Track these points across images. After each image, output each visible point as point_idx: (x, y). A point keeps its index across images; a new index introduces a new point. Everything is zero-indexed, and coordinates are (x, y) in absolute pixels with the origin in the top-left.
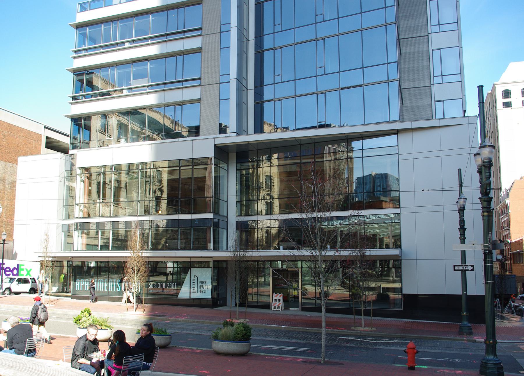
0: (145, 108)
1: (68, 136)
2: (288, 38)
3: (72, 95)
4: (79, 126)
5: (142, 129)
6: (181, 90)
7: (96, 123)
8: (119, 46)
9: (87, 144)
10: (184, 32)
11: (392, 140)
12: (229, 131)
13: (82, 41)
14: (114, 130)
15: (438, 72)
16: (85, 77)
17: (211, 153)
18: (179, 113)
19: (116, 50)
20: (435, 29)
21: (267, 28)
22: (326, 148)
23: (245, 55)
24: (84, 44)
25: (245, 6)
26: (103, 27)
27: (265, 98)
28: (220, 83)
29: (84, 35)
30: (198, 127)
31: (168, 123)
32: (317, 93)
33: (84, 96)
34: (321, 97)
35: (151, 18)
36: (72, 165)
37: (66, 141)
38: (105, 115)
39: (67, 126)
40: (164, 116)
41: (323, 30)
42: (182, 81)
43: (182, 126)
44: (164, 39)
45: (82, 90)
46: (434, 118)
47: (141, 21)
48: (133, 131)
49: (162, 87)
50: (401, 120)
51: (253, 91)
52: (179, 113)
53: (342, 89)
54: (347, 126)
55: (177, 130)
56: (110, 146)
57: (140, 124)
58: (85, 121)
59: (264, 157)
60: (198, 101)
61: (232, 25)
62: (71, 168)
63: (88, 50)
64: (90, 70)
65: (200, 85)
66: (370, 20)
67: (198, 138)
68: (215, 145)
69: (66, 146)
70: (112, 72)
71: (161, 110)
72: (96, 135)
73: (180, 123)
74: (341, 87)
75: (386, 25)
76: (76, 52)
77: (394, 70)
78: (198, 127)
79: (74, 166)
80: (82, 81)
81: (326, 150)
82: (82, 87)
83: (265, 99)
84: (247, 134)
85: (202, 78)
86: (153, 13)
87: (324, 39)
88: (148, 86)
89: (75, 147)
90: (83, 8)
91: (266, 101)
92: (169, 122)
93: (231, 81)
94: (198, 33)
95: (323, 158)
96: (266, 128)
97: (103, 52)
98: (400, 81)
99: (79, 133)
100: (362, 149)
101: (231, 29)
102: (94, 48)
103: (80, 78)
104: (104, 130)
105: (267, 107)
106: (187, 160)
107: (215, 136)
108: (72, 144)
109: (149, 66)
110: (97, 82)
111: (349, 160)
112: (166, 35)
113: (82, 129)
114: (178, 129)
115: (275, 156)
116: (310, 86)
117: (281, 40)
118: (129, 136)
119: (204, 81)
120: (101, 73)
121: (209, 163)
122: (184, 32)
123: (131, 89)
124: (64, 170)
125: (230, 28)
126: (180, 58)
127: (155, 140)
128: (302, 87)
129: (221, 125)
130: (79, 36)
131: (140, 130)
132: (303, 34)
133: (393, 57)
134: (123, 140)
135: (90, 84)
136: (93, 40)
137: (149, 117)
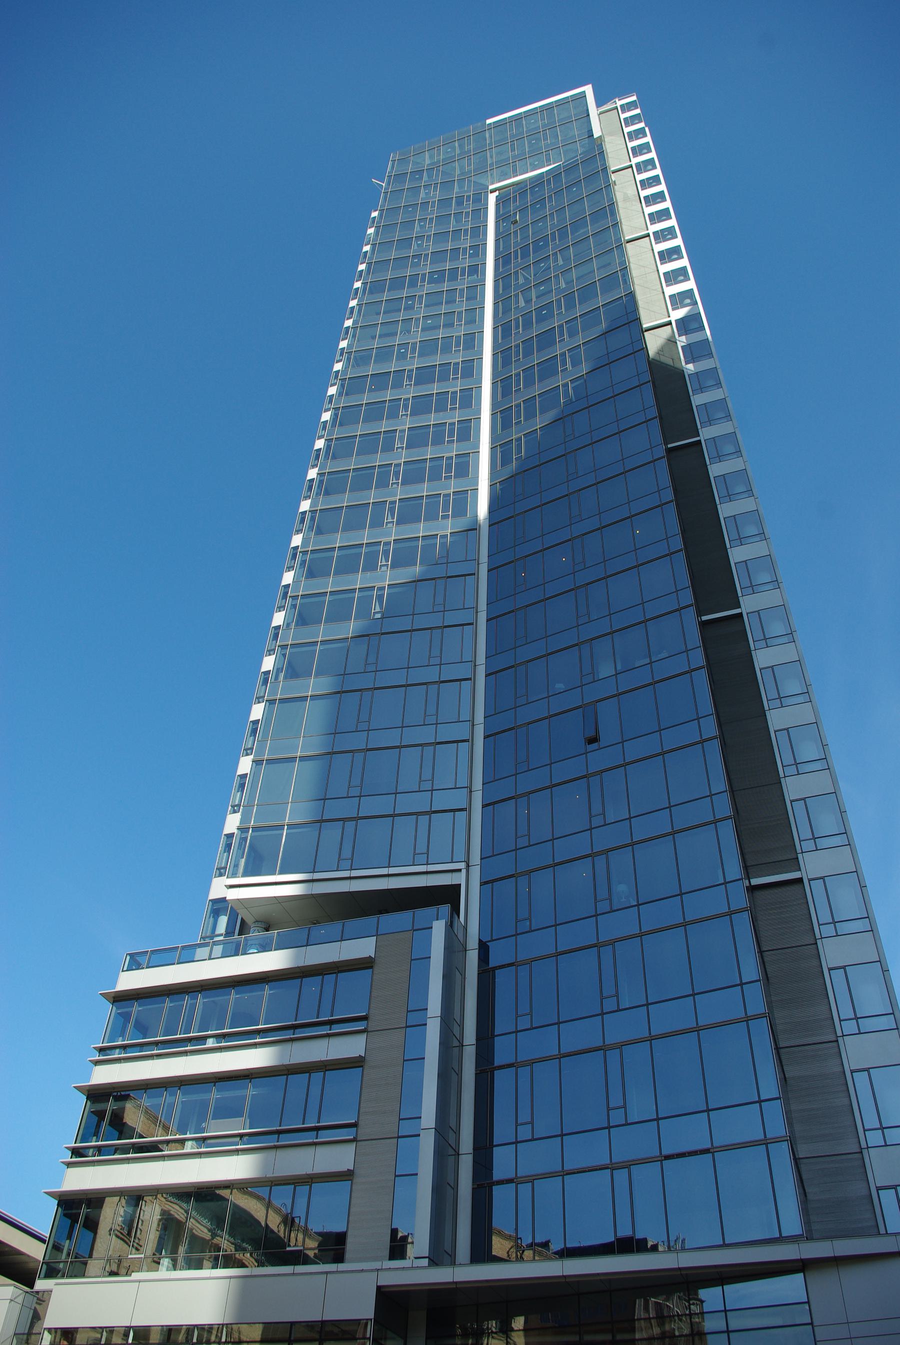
0: (229, 1185)
1: (42, 1240)
2: (544, 1043)
3: (73, 1145)
4: (74, 1219)
5: (214, 1235)
6: (310, 1150)
7: (112, 1215)
8: (192, 1044)
9: (77, 1267)
10: (331, 1023)
11: (791, 1287)
12: (411, 1251)
13: (118, 1029)
14: (150, 1233)
15: (871, 1120)
16: (110, 1106)
17: (365, 1309)
18: (301, 1202)
19: (185, 1053)
20: (828, 930)
21: (502, 1129)
22: (640, 1303)
23: (454, 1077)
24: (122, 1034)
25: (457, 973)
26: (168, 1004)
27: (497, 1176)
28: (399, 1137)
29: (126, 1017)
30: (340, 1239)
31: (274, 1222)
32: (612, 1167)
33: (100, 1150)
34: (621, 1176)
35: (267, 991)
36: (37, 1317)
37: (36, 1251)
38: (136, 1197)
39: (44, 1217)
40: (269, 1205)
41: (618, 1029)
42: (317, 1129)
43: (306, 1232)
44: (289, 1035)
45: (96, 1134)
46: (882, 1231)
47: (246, 996)
48: (195, 1240)
49: (272, 1141)
50: (809, 1236)
51: (471, 1157)
52: (301, 1202)
53: (668, 1157)
54: (683, 1249)
55: (293, 1242)
56: (135, 1276)
57: (211, 1220)
58: (88, 1207)
59: (493, 1325)
60: (347, 1175)
61: (429, 1014)
62: (32, 1326)
63: (128, 1049)
64: (120, 1093)
65: (354, 1140)
66: (714, 1008)
67: (341, 1267)
68: (379, 1288)
69: (32, 1265)
70: (170, 1099)
71: (263, 1192)
72: (106, 1243)
73: (303, 1224)
74: (664, 1152)
75: (747, 1019)
76: (101, 1050)
77: (775, 1114)
78: (340, 1239)
79: (40, 1319)
80: (100, 1115)
81: (639, 1312)
82: (98, 1126)
83: (496, 1064)
84: (453, 1263)
85: (371, 1017)
86: (272, 981)
87: (620, 1046)
88: (241, 1136)
89: (52, 1272)
90: (135, 963)
91: (501, 1067)
92: (278, 1219)
93: (422, 1133)
94: (360, 1026)
95: (633, 1330)
96: (499, 1246)
97: (159, 1056)
98: (770, 1017)
99: (70, 1237)
100: (725, 1311)
101: (429, 1021)
102: (141, 1046)
103: (100, 1106)
104: (128, 1232)
105: (501, 1196)
106: (310, 1325)
107: (377, 1265)
108: (47, 1264)
109: (250, 1091)
110: (133, 1116)
111: (696, 1338)
112: (294, 1027)
113: (104, 1124)
114: (297, 1242)
115: (519, 1323)
116: (595, 1150)
117: (534, 1045)
118: (182, 1250)
119: (364, 1131)
120: (146, 1101)
121: (359, 1334)
122: (331, 1023)
123: (204, 1139)
124: (12, 1333)
125: (426, 1018)
126: (317, 1076)
127: (243, 1265)
128: (579, 1153)
129: (394, 1232)
130: (115, 1018)
131: (207, 1235)
132: (577, 1036)
133: (770, 1087)
134: (166, 1262)
135: (119, 1126)
136: (142, 1028)
137: (236, 1207)
